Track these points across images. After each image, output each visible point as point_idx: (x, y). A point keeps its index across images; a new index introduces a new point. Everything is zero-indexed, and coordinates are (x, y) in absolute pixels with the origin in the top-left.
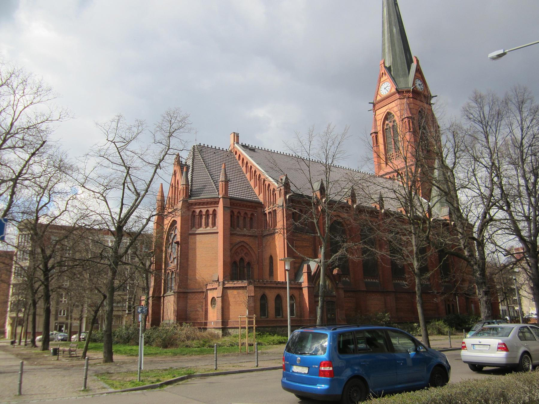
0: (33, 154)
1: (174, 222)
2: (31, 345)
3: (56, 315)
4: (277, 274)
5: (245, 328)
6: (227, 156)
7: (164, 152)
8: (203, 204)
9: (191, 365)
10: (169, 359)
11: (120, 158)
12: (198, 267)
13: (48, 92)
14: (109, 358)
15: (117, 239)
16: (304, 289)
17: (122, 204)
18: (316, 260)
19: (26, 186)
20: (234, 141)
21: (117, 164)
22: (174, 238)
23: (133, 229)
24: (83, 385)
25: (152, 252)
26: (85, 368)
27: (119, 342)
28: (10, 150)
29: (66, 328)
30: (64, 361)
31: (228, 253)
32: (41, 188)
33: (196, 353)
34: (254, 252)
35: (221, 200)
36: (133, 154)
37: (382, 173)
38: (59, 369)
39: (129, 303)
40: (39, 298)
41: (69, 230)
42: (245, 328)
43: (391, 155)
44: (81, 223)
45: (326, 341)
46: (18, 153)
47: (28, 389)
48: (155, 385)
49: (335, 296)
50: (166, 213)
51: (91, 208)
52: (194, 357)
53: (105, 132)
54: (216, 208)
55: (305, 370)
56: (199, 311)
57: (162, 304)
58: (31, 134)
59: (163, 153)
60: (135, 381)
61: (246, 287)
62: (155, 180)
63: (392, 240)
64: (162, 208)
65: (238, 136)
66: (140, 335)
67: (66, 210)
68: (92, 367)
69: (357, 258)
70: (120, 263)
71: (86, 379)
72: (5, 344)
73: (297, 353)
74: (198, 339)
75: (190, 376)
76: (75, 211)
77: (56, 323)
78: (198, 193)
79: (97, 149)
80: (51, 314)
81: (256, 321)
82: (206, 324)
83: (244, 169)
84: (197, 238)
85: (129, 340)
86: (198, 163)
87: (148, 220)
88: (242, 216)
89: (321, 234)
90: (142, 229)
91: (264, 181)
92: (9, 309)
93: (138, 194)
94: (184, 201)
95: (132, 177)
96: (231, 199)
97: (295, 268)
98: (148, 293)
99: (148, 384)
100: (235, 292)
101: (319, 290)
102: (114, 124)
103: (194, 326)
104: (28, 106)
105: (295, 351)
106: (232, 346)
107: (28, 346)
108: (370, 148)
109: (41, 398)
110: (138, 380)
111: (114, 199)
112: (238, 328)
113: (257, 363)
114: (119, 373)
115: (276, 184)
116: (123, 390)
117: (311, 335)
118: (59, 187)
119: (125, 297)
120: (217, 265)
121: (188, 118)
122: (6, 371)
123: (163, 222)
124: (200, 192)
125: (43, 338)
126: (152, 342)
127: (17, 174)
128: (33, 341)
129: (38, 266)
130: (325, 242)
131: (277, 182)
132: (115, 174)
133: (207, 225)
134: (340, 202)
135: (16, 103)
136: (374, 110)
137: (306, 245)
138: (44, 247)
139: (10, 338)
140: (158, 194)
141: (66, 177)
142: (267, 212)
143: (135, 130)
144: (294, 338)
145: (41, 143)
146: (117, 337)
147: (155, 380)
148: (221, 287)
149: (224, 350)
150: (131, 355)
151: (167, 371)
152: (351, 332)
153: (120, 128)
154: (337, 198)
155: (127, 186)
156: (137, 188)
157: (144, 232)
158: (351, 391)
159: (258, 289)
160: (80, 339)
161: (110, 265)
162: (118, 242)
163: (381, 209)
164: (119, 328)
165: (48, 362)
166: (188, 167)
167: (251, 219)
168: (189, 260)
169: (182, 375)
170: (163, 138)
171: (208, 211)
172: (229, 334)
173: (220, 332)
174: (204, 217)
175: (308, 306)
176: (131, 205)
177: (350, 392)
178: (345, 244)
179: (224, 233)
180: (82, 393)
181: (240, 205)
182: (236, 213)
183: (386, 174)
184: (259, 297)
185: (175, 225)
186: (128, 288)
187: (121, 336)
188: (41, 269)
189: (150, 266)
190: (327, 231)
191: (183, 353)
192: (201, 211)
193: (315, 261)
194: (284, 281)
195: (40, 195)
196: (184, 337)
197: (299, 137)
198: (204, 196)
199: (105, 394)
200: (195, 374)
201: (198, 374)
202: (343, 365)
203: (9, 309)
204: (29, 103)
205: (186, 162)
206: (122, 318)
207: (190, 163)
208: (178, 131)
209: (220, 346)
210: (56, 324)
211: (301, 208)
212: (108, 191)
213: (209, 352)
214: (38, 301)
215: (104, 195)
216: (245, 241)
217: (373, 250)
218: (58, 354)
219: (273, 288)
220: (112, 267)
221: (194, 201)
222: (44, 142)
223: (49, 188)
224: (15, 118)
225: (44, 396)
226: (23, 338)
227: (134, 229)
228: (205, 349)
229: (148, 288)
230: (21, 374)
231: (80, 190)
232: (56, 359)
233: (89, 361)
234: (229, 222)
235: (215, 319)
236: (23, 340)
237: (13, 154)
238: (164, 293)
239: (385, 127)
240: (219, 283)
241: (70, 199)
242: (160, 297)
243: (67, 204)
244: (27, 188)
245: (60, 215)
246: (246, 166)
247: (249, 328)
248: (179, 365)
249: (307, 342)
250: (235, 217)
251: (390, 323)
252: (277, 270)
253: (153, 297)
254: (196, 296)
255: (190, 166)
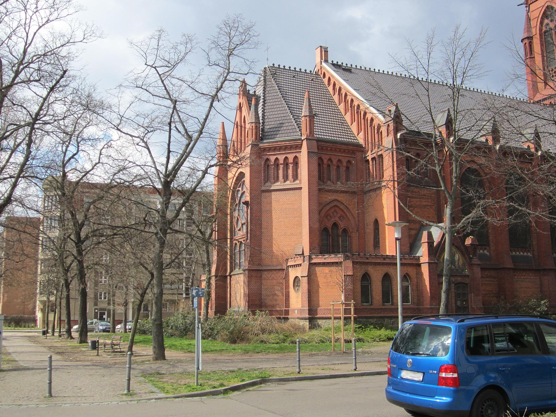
0: (52, 89)
1: (242, 175)
2: (66, 336)
3: (96, 298)
4: (385, 246)
5: (340, 318)
6: (312, 80)
7: (222, 77)
8: (280, 148)
9: (266, 366)
10: (238, 357)
11: (164, 88)
12: (275, 236)
13: (68, 4)
14: (160, 355)
15: (165, 199)
16: (422, 266)
17: (169, 152)
18: (440, 224)
19: (47, 132)
20: (321, 59)
21: (160, 97)
22: (241, 198)
23: (187, 185)
24: (126, 387)
25: (213, 217)
26: (127, 366)
27: (175, 334)
28: (24, 84)
29: (109, 316)
30: (105, 357)
31: (316, 217)
32: (67, 134)
33: (274, 351)
34: (352, 215)
35: (305, 143)
36: (181, 82)
37: (538, 97)
38: (98, 367)
39: (187, 285)
40: (73, 278)
41: (107, 188)
42: (340, 318)
43: (552, 70)
44: (123, 177)
45: (449, 338)
46: (33, 88)
47: (60, 390)
48: (217, 391)
49: (468, 276)
50: (229, 163)
51: (130, 159)
52: (271, 356)
53: (143, 53)
54: (297, 155)
55: (418, 377)
56: (278, 296)
57: (229, 286)
58: (48, 62)
59: (222, 79)
60: (192, 384)
61: (341, 263)
62: (212, 117)
63: (551, 195)
64: (225, 156)
65: (326, 52)
66: (196, 326)
67: (99, 163)
68: (138, 365)
69: (499, 221)
70: (169, 231)
71: (129, 380)
72: (36, 334)
73: (408, 354)
74: (277, 333)
75: (264, 381)
76: (111, 162)
77: (95, 309)
78: (272, 133)
79: (133, 78)
80: (88, 297)
81: (355, 310)
82: (287, 312)
83: (336, 98)
84: (273, 197)
85: (186, 332)
86: (272, 91)
87: (205, 172)
88: (335, 165)
89: (446, 188)
90: (197, 185)
91: (365, 113)
92: (38, 291)
93: (190, 137)
94: (253, 146)
95: (180, 114)
96: (318, 141)
97: (410, 236)
98: (210, 271)
99: (208, 390)
100: (326, 269)
101: (443, 267)
102: (154, 43)
103: (271, 315)
104: (43, 25)
105: (406, 350)
106: (323, 342)
107: (63, 337)
108: (519, 60)
109: (74, 402)
110: (196, 384)
111: (158, 144)
112: (330, 318)
113: (356, 365)
114: (172, 374)
115: (381, 117)
116: (176, 395)
117: (428, 329)
118: (90, 131)
119: (181, 275)
120: (301, 233)
121: (254, 28)
122: (35, 367)
123: (226, 176)
124: (275, 133)
125: (79, 327)
126: (216, 334)
127: (34, 117)
128: (69, 332)
129: (69, 237)
130: (452, 199)
131: (382, 112)
132: (159, 111)
133: (286, 178)
134: (473, 142)
135: (28, 21)
136: (527, 4)
137: (425, 203)
138: (75, 211)
139: (41, 328)
140: (218, 136)
141: (97, 118)
142: (369, 158)
143: (182, 48)
144: (404, 331)
145: (61, 73)
146: (172, 328)
147: (218, 384)
148: (307, 263)
149: (311, 348)
150: (189, 352)
151: (234, 373)
152: (486, 325)
153: (162, 47)
154: (469, 136)
155: (176, 127)
156: (189, 129)
157: (202, 188)
158: (484, 407)
159: (358, 266)
160: (126, 329)
161: (156, 234)
162: (166, 204)
163: (537, 150)
164: (174, 316)
165: (87, 358)
166: (258, 99)
167: (348, 168)
168: (263, 226)
169: (253, 378)
170: (220, 57)
171: (286, 158)
172: (319, 326)
173: (307, 324)
174: (281, 166)
175: (428, 290)
176: (181, 152)
177: (482, 408)
178: (482, 202)
179: (309, 189)
180: (124, 397)
181: (327, 149)
182: (325, 161)
183: (544, 99)
184: (359, 278)
185: (242, 179)
186: (184, 264)
187: (176, 327)
188: (72, 240)
189: (211, 235)
190: (454, 183)
191: (257, 351)
192: (277, 159)
193: (439, 227)
194: (395, 255)
195: (66, 143)
196: (258, 330)
197: (413, 47)
198: (281, 138)
199: (154, 400)
200: (271, 378)
201: (274, 377)
202: (474, 371)
203: (38, 291)
204: (44, 20)
205: (255, 92)
206: (178, 303)
207: (260, 91)
208: (241, 47)
209: (306, 342)
210: (96, 311)
211: (419, 152)
212: (149, 134)
213: (292, 350)
214: (71, 281)
215: (145, 140)
216: (340, 199)
217: (523, 209)
218: (98, 347)
219: (379, 264)
220: (159, 236)
221: (267, 144)
222: (65, 72)
223: (77, 133)
224: (29, 42)
225: (79, 399)
226: (57, 327)
227: (188, 186)
228: (287, 346)
229: (209, 265)
230: (50, 371)
231: (115, 134)
232: (96, 354)
233: (133, 358)
234: (316, 173)
235: (299, 306)
236: (57, 330)
237: (26, 89)
238: (231, 271)
239: (544, 29)
240: (304, 257)
241: (103, 148)
242: (226, 277)
243: (101, 154)
244: (49, 135)
245: (93, 169)
246: (339, 94)
247: (345, 318)
248: (251, 365)
249: (423, 337)
250: (325, 166)
251: (547, 314)
252: (385, 239)
253: (216, 276)
254: (273, 276)
255: (260, 97)
